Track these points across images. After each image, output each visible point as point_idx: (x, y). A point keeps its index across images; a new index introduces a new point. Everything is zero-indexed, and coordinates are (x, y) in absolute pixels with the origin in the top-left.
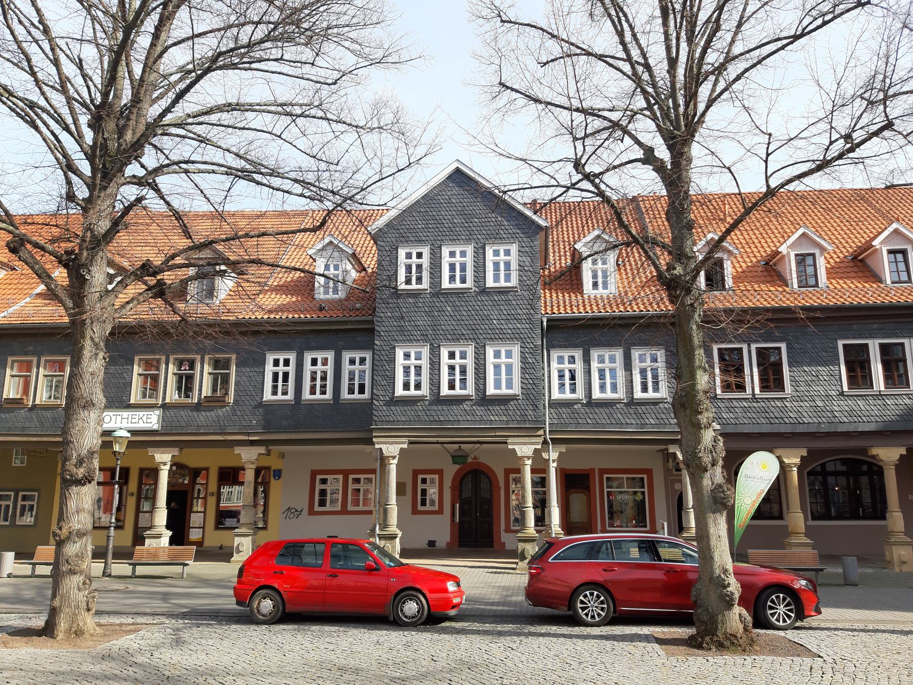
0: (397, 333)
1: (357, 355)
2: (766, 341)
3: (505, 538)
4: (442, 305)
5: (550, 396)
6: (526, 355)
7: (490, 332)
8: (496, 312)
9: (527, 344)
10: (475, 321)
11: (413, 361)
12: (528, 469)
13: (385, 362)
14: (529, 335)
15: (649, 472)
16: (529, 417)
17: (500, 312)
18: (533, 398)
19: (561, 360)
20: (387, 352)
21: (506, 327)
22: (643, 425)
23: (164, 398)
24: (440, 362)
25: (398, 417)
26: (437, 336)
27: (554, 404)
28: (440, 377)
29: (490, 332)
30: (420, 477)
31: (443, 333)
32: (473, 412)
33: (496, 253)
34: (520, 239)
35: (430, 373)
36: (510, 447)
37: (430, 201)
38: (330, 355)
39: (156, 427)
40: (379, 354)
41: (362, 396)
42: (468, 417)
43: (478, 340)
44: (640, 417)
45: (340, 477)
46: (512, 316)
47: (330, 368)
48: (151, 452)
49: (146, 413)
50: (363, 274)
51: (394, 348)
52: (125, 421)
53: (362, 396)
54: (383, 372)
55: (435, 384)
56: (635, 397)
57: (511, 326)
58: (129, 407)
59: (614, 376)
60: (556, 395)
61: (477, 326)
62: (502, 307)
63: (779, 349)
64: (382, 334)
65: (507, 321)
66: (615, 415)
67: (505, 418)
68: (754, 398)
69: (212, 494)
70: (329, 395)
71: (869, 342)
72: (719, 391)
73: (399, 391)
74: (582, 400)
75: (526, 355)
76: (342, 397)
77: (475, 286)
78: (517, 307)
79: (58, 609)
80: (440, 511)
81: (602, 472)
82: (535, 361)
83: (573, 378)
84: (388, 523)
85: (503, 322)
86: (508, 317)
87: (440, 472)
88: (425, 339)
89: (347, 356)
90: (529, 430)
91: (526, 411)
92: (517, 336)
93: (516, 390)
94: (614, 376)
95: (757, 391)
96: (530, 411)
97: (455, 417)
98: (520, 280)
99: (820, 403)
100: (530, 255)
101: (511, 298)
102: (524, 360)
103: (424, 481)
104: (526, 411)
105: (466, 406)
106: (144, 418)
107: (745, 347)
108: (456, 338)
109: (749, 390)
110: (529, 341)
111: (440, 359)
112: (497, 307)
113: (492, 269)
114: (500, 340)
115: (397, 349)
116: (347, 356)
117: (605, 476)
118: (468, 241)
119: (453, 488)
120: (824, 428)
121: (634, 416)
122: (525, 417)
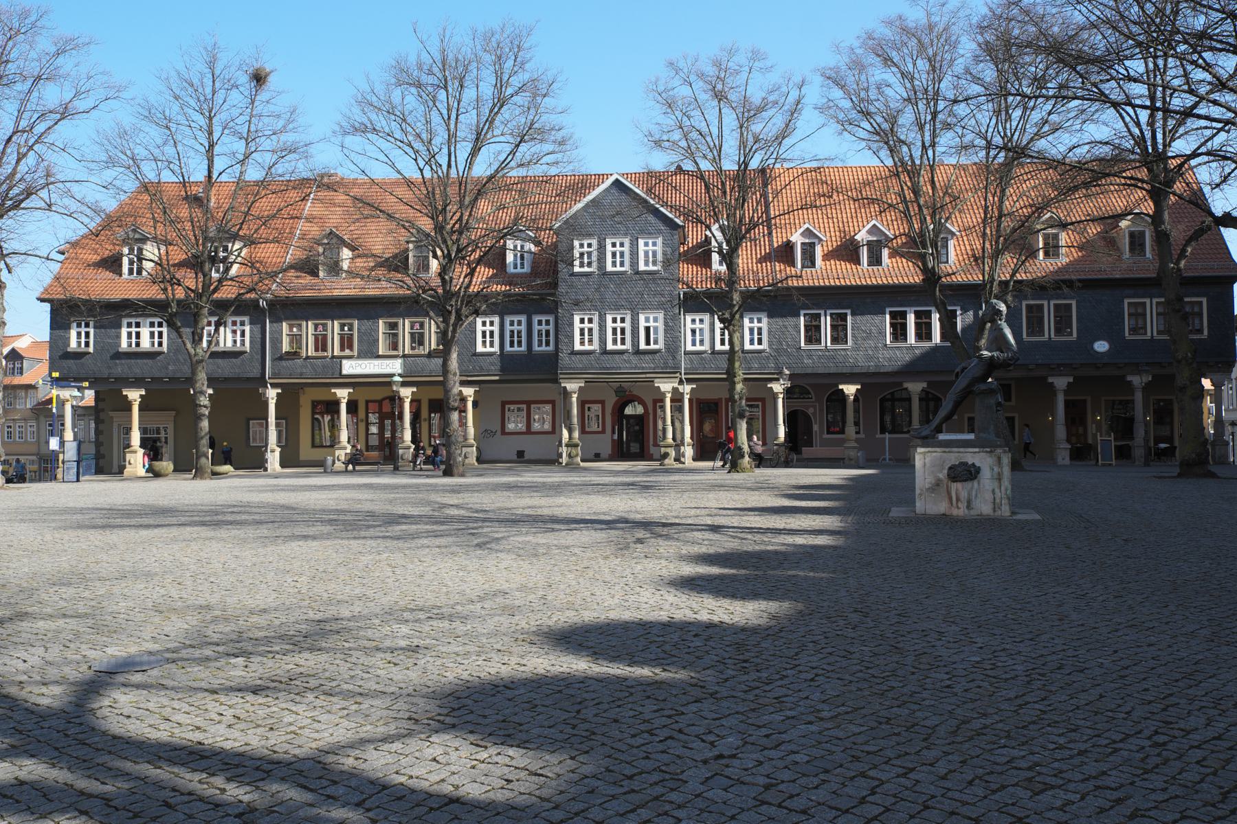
1: (544, 318)
2: (837, 308)
3: (652, 450)
11: (488, 328)
19: (751, 321)
22: (750, 369)
23: (404, 351)
30: (587, 406)
33: (646, 244)
38: (523, 318)
41: (548, 348)
45: (524, 406)
47: (523, 328)
53: (548, 348)
55: (603, 341)
58: (379, 357)
59: (701, 334)
60: (690, 348)
63: (1201, 303)
69: (425, 420)
70: (524, 348)
71: (907, 309)
73: (578, 347)
80: (603, 432)
83: (760, 333)
87: (602, 403)
89: (536, 319)
90: (670, 371)
93: (661, 345)
94: (701, 334)
95: (829, 344)
99: (870, 352)
102: (666, 324)
105: (625, 357)
108: (617, 308)
109: (1047, 335)
116: (536, 319)
118: (626, 235)
119: (613, 414)
120: (872, 370)
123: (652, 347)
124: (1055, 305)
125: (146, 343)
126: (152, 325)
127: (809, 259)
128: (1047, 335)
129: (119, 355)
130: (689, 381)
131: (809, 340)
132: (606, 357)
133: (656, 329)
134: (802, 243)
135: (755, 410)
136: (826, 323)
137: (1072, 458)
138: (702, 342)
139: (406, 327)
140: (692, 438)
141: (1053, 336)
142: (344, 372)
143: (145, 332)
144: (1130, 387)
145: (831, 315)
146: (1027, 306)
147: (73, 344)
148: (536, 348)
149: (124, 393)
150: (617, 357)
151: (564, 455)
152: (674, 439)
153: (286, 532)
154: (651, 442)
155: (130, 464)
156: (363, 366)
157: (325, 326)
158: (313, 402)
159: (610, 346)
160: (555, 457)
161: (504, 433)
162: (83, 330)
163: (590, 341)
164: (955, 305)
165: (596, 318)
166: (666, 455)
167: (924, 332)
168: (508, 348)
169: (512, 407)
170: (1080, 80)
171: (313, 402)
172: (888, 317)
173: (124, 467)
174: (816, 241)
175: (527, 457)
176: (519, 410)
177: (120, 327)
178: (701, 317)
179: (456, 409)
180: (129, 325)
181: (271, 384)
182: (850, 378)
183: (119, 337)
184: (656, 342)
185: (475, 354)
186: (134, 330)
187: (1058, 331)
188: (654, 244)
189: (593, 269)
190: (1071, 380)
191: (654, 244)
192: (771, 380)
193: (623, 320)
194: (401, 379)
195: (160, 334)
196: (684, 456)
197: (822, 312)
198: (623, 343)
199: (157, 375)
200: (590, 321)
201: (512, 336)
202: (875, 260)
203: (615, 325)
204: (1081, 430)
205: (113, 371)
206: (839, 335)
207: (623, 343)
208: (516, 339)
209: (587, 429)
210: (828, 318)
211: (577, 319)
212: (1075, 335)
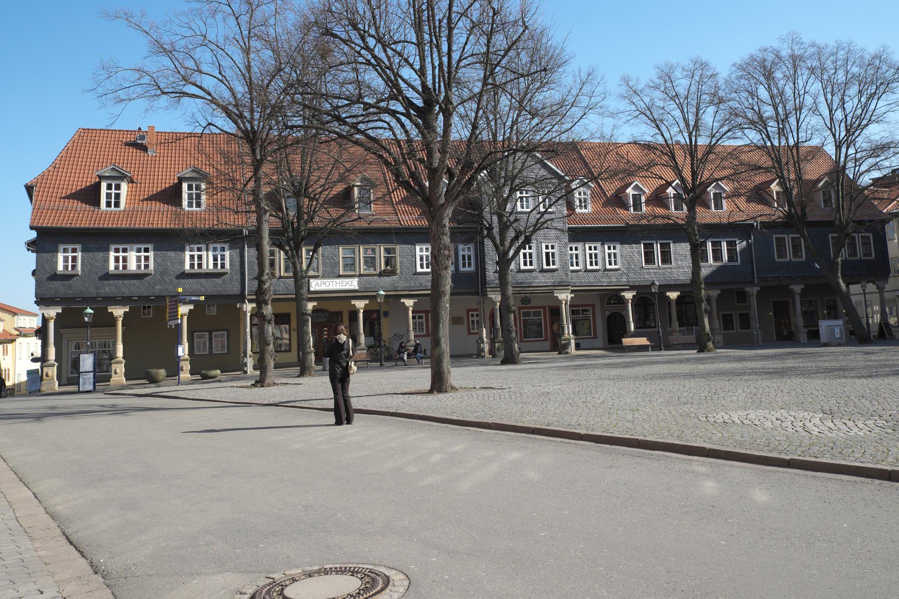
15: (593, 306)
30: (470, 313)
36: (555, 295)
39: (357, 288)
48: (353, 302)
49: (350, 280)
52: (338, 285)
58: (339, 276)
68: (659, 268)
70: (472, 268)
72: (644, 265)
103: (473, 315)
105: (533, 274)
106: (349, 283)
107: (786, 236)
109: (788, 258)
123: (552, 267)
124: (791, 237)
125: (132, 266)
126: (139, 251)
127: (637, 205)
128: (788, 258)
129: (107, 276)
131: (647, 262)
134: (633, 195)
136: (657, 249)
137: (809, 339)
139: (362, 252)
141: (792, 258)
142: (312, 289)
143: (132, 256)
144: (791, 293)
145: (660, 243)
146: (776, 238)
147: (60, 267)
148: (462, 269)
155: (116, 373)
156: (327, 284)
157: (373, 250)
158: (467, 310)
159: (589, 267)
161: (469, 333)
162: (70, 255)
164: (735, 237)
167: (717, 256)
170: (253, 30)
171: (467, 310)
172: (642, 245)
173: (110, 376)
174: (641, 193)
177: (108, 250)
178: (595, 245)
180: (117, 251)
181: (248, 300)
182: (673, 287)
183: (107, 260)
185: (416, 274)
186: (121, 254)
187: (795, 255)
190: (803, 287)
192: (624, 290)
194: (384, 293)
195: (147, 258)
196: (246, 366)
197: (655, 242)
198: (577, 265)
199: (144, 294)
202: (718, 206)
203: (591, 252)
204: (787, 321)
205: (102, 291)
206: (666, 258)
207: (531, 264)
208: (467, 261)
209: (472, 331)
210: (659, 245)
212: (804, 257)
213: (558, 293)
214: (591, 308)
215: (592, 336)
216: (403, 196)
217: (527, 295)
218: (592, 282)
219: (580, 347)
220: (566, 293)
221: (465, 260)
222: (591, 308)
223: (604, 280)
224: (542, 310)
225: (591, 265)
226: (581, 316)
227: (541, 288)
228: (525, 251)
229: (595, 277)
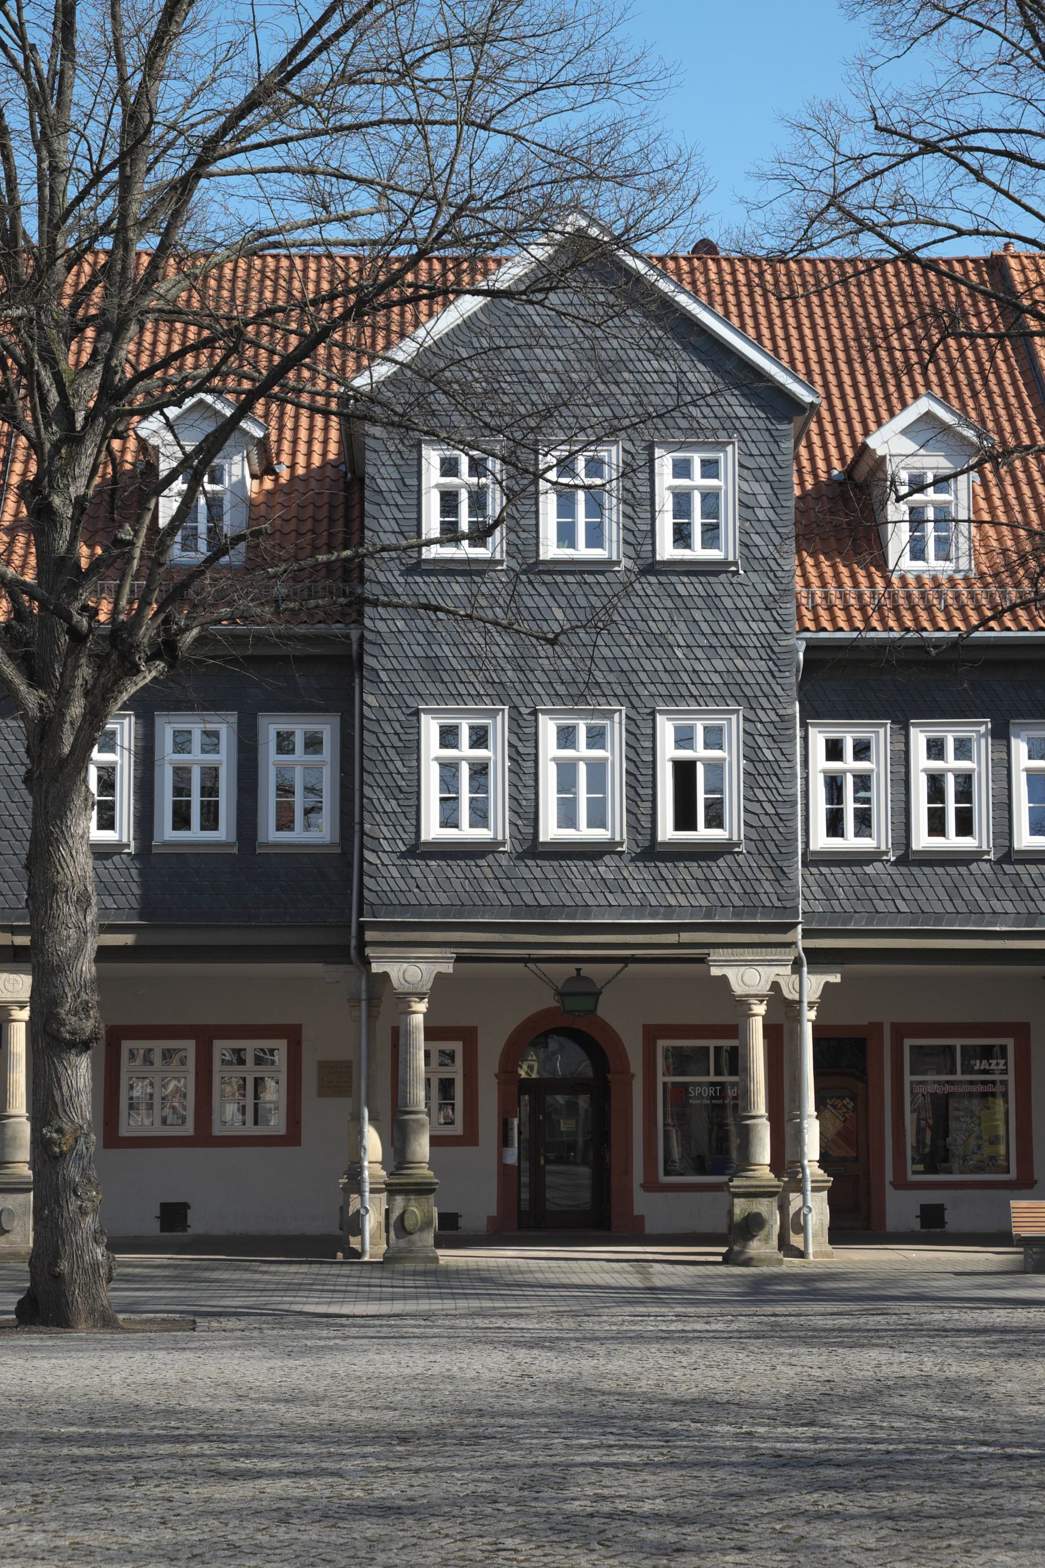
0: (423, 674)
1: (299, 727)
4: (542, 604)
5: (807, 843)
6: (759, 740)
7: (666, 678)
8: (682, 626)
9: (760, 713)
10: (626, 650)
11: (196, 758)
12: (757, 1026)
13: (390, 751)
14: (767, 689)
16: (764, 897)
17: (692, 626)
18: (774, 850)
20: (397, 725)
21: (709, 667)
24: (536, 755)
25: (431, 895)
26: (529, 687)
27: (814, 860)
28: (537, 794)
29: (666, 678)
31: (544, 679)
32: (622, 882)
33: (682, 469)
34: (745, 434)
35: (512, 785)
36: (715, 971)
37: (507, 320)
38: (225, 727)
40: (377, 729)
41: (209, 836)
42: (609, 896)
43: (636, 701)
44: (1025, 896)
45: (189, 1046)
46: (723, 639)
47: (225, 759)
50: (268, 484)
51: (417, 713)
53: (209, 836)
54: (387, 778)
56: (1017, 846)
57: (719, 665)
60: (821, 841)
61: (635, 663)
62: (697, 615)
64: (383, 676)
65: (711, 652)
66: (965, 892)
67: (704, 902)
70: (224, 832)
73: (432, 830)
74: (886, 853)
75: (759, 740)
76: (261, 838)
77: (626, 556)
78: (735, 614)
79: (67, 1278)
81: (901, 1031)
82: (780, 757)
83: (964, 794)
84: (410, 1158)
85: (699, 652)
86: (714, 641)
88: (500, 693)
89: (270, 727)
91: (755, 884)
92: (736, 691)
96: (766, 884)
97: (578, 898)
98: (744, 545)
100: (771, 478)
101: (720, 591)
102: (752, 754)
104: (755, 884)
105: (605, 868)
110: (766, 705)
111: (536, 747)
112: (685, 612)
113: (669, 505)
114: (691, 701)
115: (423, 717)
116: (270, 727)
117: (908, 1042)
121: (1011, 892)
122: (754, 897)
123: (703, 833)
130: (818, 959)
132: (535, 869)
133: (715, 768)
135: (994, 1064)
138: (863, 820)
140: (824, 1161)
148: (270, 833)
149: (376, 968)
150: (574, 868)
151: (372, 1222)
152: (777, 1166)
153: (326, 1414)
154: (638, 1175)
159: (922, 840)
160: (334, 1229)
163: (863, 820)
165: (499, 728)
166: (753, 1225)
168: (166, 832)
169: (141, 1045)
175: (197, 1224)
176: (168, 1055)
178: (863, 734)
179: (84, 1046)
184: (715, 820)
188: (710, 468)
189: (494, 548)
191: (710, 468)
193: (480, 738)
196: (359, 1231)
200: (480, 738)
201: (181, 789)
207: (965, 827)
211: (430, 728)
213: (728, 963)
214: (1010, 1043)
215: (1013, 1175)
216: (823, 477)
217: (587, 969)
218: (938, 918)
219: (941, 1223)
220: (770, 963)
221: (840, 800)
222: (1010, 1043)
223: (998, 906)
224: (908, 1042)
225: (937, 827)
226: (959, 1077)
227: (672, 938)
228: (107, 757)
229: (953, 892)
